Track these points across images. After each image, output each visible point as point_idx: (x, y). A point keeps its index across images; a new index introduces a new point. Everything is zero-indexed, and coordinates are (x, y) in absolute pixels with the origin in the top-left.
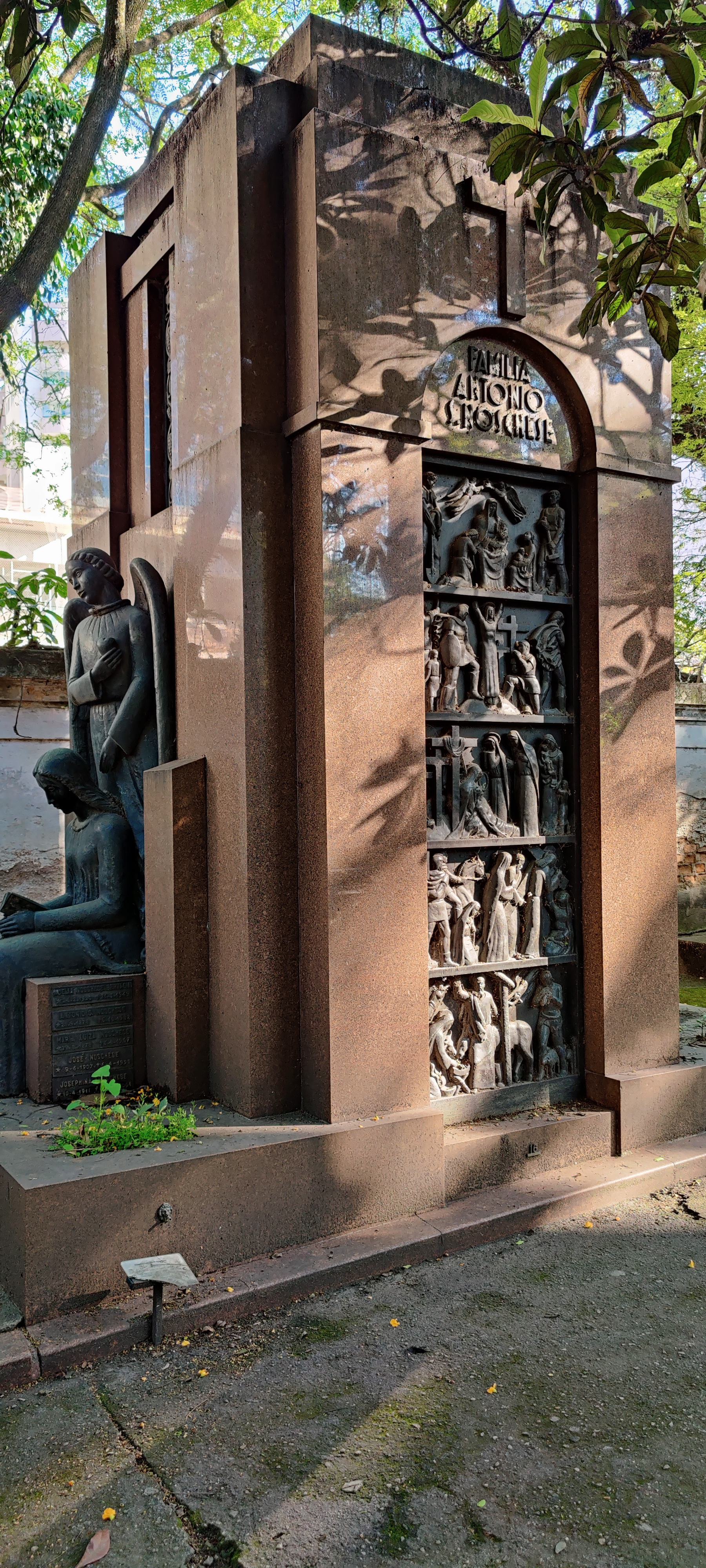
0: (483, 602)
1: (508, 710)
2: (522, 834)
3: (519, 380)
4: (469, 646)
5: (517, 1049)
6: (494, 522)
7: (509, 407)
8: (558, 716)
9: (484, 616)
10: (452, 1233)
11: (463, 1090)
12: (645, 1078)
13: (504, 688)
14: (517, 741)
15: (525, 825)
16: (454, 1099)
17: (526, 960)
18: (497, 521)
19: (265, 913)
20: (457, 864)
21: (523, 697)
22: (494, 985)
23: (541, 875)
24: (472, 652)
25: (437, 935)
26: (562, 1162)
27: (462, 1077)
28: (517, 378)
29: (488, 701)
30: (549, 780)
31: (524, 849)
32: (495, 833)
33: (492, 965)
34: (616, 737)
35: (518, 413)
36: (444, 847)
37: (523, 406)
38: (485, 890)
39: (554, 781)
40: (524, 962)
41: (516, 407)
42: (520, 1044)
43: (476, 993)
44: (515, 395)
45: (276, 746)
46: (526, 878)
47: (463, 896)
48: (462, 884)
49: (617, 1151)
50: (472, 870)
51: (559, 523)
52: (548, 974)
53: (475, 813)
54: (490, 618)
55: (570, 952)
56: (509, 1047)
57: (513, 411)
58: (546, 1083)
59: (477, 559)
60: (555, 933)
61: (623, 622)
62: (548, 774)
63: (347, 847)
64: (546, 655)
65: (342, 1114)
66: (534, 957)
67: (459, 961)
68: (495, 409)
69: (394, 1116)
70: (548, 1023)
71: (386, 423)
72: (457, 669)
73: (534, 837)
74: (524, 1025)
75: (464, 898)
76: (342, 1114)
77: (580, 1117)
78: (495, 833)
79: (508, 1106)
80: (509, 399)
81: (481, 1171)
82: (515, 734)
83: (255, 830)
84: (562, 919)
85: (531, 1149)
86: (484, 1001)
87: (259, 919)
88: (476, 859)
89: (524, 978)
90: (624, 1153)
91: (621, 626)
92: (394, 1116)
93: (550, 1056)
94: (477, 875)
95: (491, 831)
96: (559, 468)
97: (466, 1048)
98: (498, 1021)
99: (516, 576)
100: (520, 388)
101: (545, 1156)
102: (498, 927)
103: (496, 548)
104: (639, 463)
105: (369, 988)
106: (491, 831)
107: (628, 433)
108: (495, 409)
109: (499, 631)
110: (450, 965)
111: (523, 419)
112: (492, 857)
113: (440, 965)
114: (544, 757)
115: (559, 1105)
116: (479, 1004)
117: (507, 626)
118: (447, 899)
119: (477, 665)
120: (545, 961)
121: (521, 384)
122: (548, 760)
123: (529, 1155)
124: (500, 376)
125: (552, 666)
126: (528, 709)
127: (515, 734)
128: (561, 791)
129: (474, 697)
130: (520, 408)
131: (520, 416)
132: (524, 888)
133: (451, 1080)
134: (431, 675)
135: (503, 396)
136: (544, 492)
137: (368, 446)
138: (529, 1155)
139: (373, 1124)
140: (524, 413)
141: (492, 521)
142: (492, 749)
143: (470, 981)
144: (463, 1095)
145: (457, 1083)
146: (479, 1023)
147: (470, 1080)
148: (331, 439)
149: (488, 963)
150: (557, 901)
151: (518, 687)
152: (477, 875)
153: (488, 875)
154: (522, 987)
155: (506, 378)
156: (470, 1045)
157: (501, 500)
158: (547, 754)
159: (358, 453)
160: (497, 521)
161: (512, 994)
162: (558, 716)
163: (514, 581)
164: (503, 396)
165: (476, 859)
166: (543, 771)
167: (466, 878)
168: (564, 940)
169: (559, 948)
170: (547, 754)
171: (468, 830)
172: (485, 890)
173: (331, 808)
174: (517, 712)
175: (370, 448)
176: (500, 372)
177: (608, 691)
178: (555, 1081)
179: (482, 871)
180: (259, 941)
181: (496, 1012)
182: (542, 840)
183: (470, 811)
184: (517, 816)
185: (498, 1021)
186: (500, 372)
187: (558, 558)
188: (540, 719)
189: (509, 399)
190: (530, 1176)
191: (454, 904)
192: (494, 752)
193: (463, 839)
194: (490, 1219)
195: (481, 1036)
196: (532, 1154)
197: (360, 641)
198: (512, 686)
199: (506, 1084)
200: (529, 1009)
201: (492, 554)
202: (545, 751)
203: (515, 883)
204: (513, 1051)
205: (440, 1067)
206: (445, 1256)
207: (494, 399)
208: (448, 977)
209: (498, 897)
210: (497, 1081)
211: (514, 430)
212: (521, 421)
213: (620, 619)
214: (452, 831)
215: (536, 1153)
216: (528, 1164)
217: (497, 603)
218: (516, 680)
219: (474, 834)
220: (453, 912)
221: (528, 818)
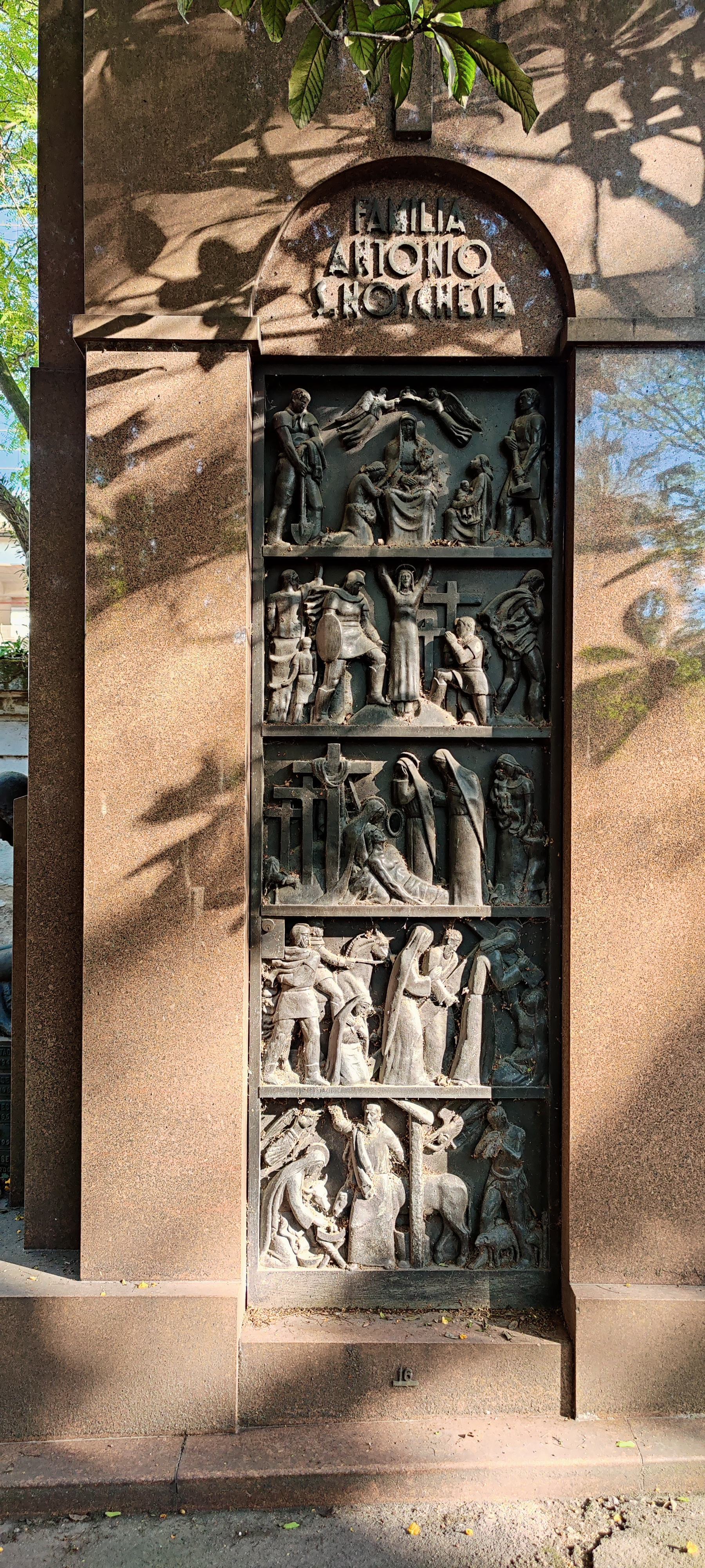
0: (395, 564)
1: (434, 718)
2: (452, 901)
3: (445, 232)
4: (371, 629)
5: (437, 1218)
6: (414, 447)
7: (425, 275)
8: (515, 724)
9: (396, 582)
10: (194, 1480)
11: (334, 1262)
12: (628, 1302)
13: (429, 688)
14: (444, 765)
15: (456, 888)
16: (314, 1273)
17: (452, 1086)
18: (417, 445)
19: (51, 987)
20: (349, 939)
21: (462, 698)
22: (400, 1119)
23: (483, 963)
24: (377, 637)
25: (299, 1038)
26: (462, 1406)
27: (334, 1244)
28: (441, 228)
29: (398, 705)
30: (507, 823)
31: (461, 924)
32: (400, 898)
33: (388, 1089)
34: (600, 759)
35: (441, 282)
36: (307, 914)
37: (450, 270)
38: (384, 978)
39: (515, 825)
40: (449, 1089)
41: (438, 274)
42: (441, 1208)
43: (362, 1126)
44: (436, 256)
45: (72, 773)
46: (462, 966)
47: (347, 986)
48: (344, 968)
49: (569, 1410)
50: (366, 948)
51: (531, 438)
52: (497, 1112)
53: (366, 869)
54: (403, 587)
55: (537, 1082)
56: (419, 1212)
57: (433, 280)
58: (484, 1273)
59: (383, 505)
60: (518, 1051)
61: (621, 576)
62: (504, 813)
63: (116, 911)
64: (509, 637)
65: (97, 1270)
66: (470, 1084)
67: (330, 1079)
68: (401, 283)
69: (164, 1287)
70: (499, 1183)
71: (191, 328)
72: (340, 665)
73: (474, 905)
74: (456, 1184)
75: (349, 988)
76: (97, 1270)
77: (503, 1341)
78: (400, 898)
79: (412, 1298)
80: (425, 264)
81: (308, 1391)
82: (443, 754)
83: (39, 880)
84: (528, 1032)
85: (401, 1374)
86: (376, 1138)
87: (42, 994)
88: (374, 933)
89: (459, 1112)
90: (580, 1416)
91: (618, 583)
92: (164, 1287)
93: (497, 1234)
94: (376, 957)
95: (394, 894)
96: (520, 353)
97: (344, 1203)
98: (404, 1170)
99: (456, 523)
100: (446, 245)
101: (427, 1390)
102: (400, 1033)
103: (411, 486)
104: (670, 322)
105: (145, 1104)
106: (394, 894)
107: (636, 276)
108: (401, 283)
109: (423, 604)
110: (314, 1082)
111: (450, 290)
112: (400, 930)
113: (302, 1082)
114: (500, 788)
115: (497, 1315)
116: (363, 1142)
117: (441, 598)
118: (318, 987)
119: (381, 655)
120: (486, 1093)
121: (449, 237)
122: (505, 793)
123: (395, 1383)
124: (410, 232)
125: (516, 653)
126: (469, 717)
127: (443, 754)
128: (527, 838)
129: (376, 702)
130: (446, 275)
131: (445, 288)
132: (459, 980)
133: (316, 1246)
134: (299, 673)
135: (414, 261)
136: (514, 395)
137: (159, 365)
138: (395, 1383)
139: (136, 1293)
140: (453, 280)
141: (408, 447)
142: (402, 776)
143: (357, 1108)
144: (335, 1269)
145: (325, 1251)
146: (362, 1171)
147: (345, 1250)
148: (104, 362)
149: (384, 1086)
150: (522, 1003)
151: (452, 685)
152: (376, 957)
153: (392, 957)
154: (453, 1124)
155: (422, 234)
156: (351, 1200)
157: (432, 413)
158: (504, 784)
159: (143, 376)
160: (417, 445)
161: (436, 1133)
162: (515, 724)
163: (396, 528)
164: (414, 261)
165: (374, 933)
166: (493, 809)
167: (353, 960)
168: (527, 1063)
169: (515, 1076)
170: (504, 784)
171: (353, 892)
172: (384, 978)
173: (92, 857)
174: (452, 721)
175: (162, 368)
176: (409, 226)
177: (587, 686)
178: (502, 1274)
179: (385, 952)
180: (42, 1022)
181: (402, 1158)
182: (485, 912)
183: (359, 865)
184: (447, 873)
185: (404, 1170)
186: (409, 226)
187: (529, 490)
188: (485, 731)
189: (425, 264)
190: (399, 1414)
191: (329, 996)
192: (407, 780)
193: (344, 903)
194: (265, 1473)
195: (365, 1190)
196: (400, 1383)
197: (142, 631)
198: (443, 684)
199: (415, 1263)
200: (462, 1160)
201: (405, 494)
202: (502, 780)
203: (437, 971)
204: (428, 1218)
205: (295, 1223)
206: (179, 1513)
207: (397, 268)
208: (307, 1100)
209: (401, 992)
210: (398, 1257)
211: (435, 307)
212: (445, 292)
213: (617, 572)
214: (325, 892)
215: (409, 1383)
216: (395, 1398)
217: (419, 565)
218: (448, 675)
219: (363, 899)
220: (329, 1008)
221: (460, 878)
